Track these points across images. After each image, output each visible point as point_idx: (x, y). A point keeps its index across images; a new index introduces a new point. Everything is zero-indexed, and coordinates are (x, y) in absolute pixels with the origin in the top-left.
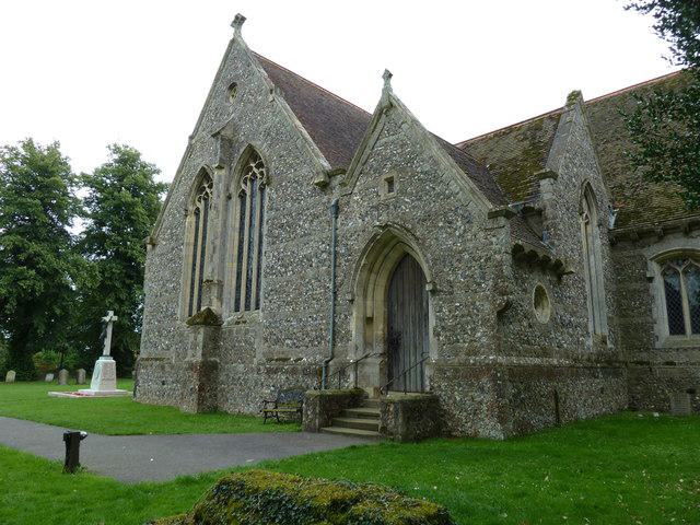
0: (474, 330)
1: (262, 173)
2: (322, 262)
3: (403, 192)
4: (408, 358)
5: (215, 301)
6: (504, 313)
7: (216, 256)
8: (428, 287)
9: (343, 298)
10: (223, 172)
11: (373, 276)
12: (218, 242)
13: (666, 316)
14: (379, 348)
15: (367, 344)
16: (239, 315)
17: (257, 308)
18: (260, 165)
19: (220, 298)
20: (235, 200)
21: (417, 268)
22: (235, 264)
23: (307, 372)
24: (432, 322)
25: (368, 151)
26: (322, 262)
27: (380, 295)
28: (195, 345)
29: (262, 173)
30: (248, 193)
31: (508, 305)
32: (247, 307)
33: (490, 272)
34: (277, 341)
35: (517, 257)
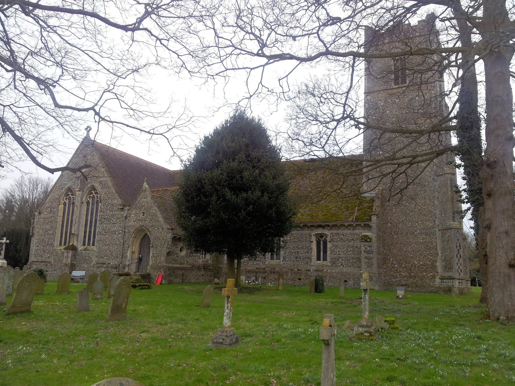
0: (161, 257)
1: (97, 196)
2: (120, 233)
3: (146, 217)
4: (143, 263)
5: (75, 241)
6: (168, 254)
7: (76, 225)
8: (151, 245)
9: (126, 246)
10: (80, 193)
11: (136, 240)
12: (77, 220)
13: (316, 255)
14: (136, 261)
15: (132, 259)
16: (85, 247)
17: (93, 245)
18: (96, 193)
19: (77, 240)
20: (85, 204)
21: (149, 238)
22: (84, 228)
23: (112, 267)
24: (151, 255)
25: (137, 202)
26: (120, 233)
27: (138, 245)
28: (67, 257)
29: (97, 196)
30: (91, 202)
31: (169, 252)
32: (89, 245)
33: (166, 243)
34: (101, 257)
35: (467, 170)
